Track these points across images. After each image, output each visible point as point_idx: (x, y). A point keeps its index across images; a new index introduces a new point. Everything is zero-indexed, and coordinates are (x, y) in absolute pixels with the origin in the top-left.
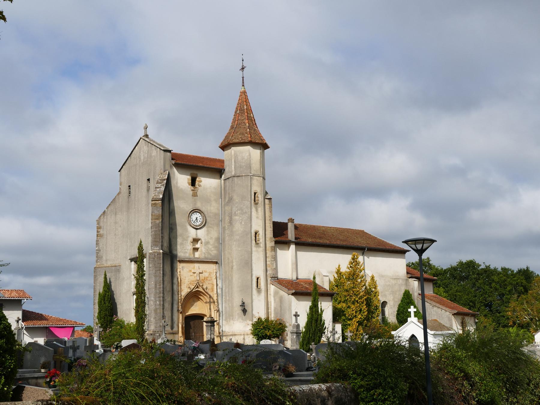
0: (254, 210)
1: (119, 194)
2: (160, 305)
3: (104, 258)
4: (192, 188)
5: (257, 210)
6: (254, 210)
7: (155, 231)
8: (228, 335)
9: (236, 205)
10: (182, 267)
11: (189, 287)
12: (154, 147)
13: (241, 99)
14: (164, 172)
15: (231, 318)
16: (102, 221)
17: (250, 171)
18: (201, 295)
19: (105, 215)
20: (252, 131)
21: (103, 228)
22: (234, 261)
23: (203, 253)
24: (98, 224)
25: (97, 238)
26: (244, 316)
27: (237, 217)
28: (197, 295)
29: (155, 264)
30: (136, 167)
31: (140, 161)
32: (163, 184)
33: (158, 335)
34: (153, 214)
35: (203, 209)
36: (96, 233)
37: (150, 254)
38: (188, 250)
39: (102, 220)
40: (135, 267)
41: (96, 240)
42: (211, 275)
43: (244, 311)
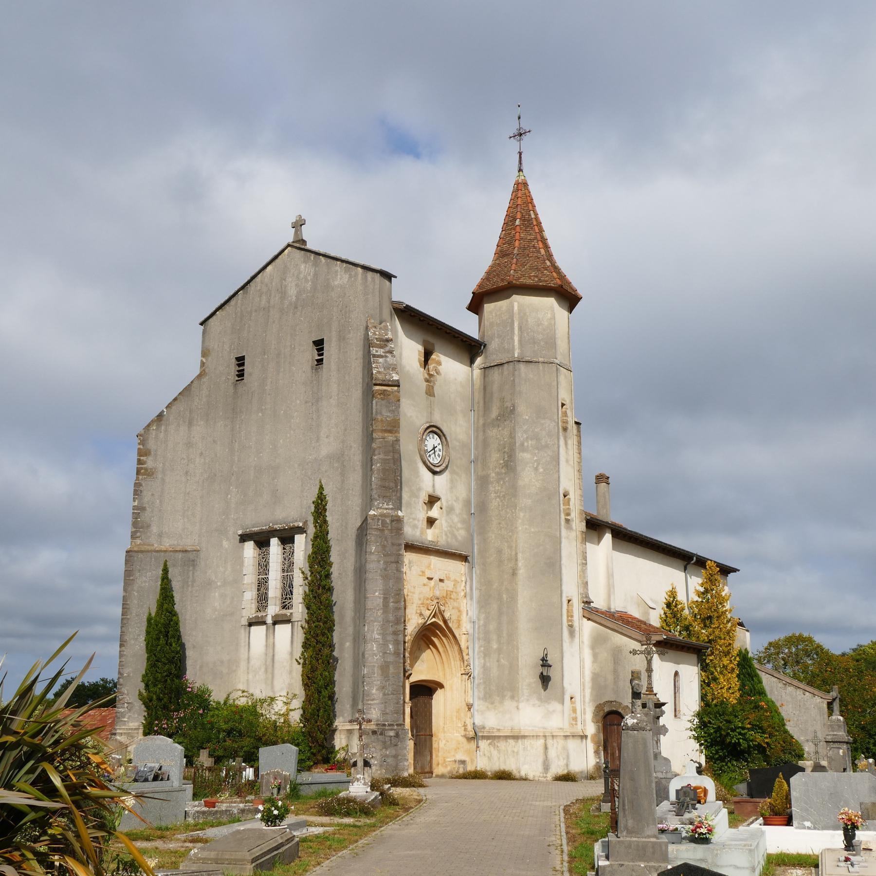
1: (200, 376)
2: (396, 653)
3: (154, 529)
8: (500, 736)
9: (525, 427)
11: (421, 614)
15: (509, 694)
18: (436, 636)
21: (156, 455)
22: (520, 556)
23: (444, 533)
24: (143, 442)
25: (137, 479)
26: (545, 691)
27: (526, 456)
28: (429, 634)
29: (384, 547)
30: (269, 311)
33: (392, 733)
36: (134, 465)
40: (255, 556)
41: (135, 483)
42: (456, 588)
43: (545, 680)
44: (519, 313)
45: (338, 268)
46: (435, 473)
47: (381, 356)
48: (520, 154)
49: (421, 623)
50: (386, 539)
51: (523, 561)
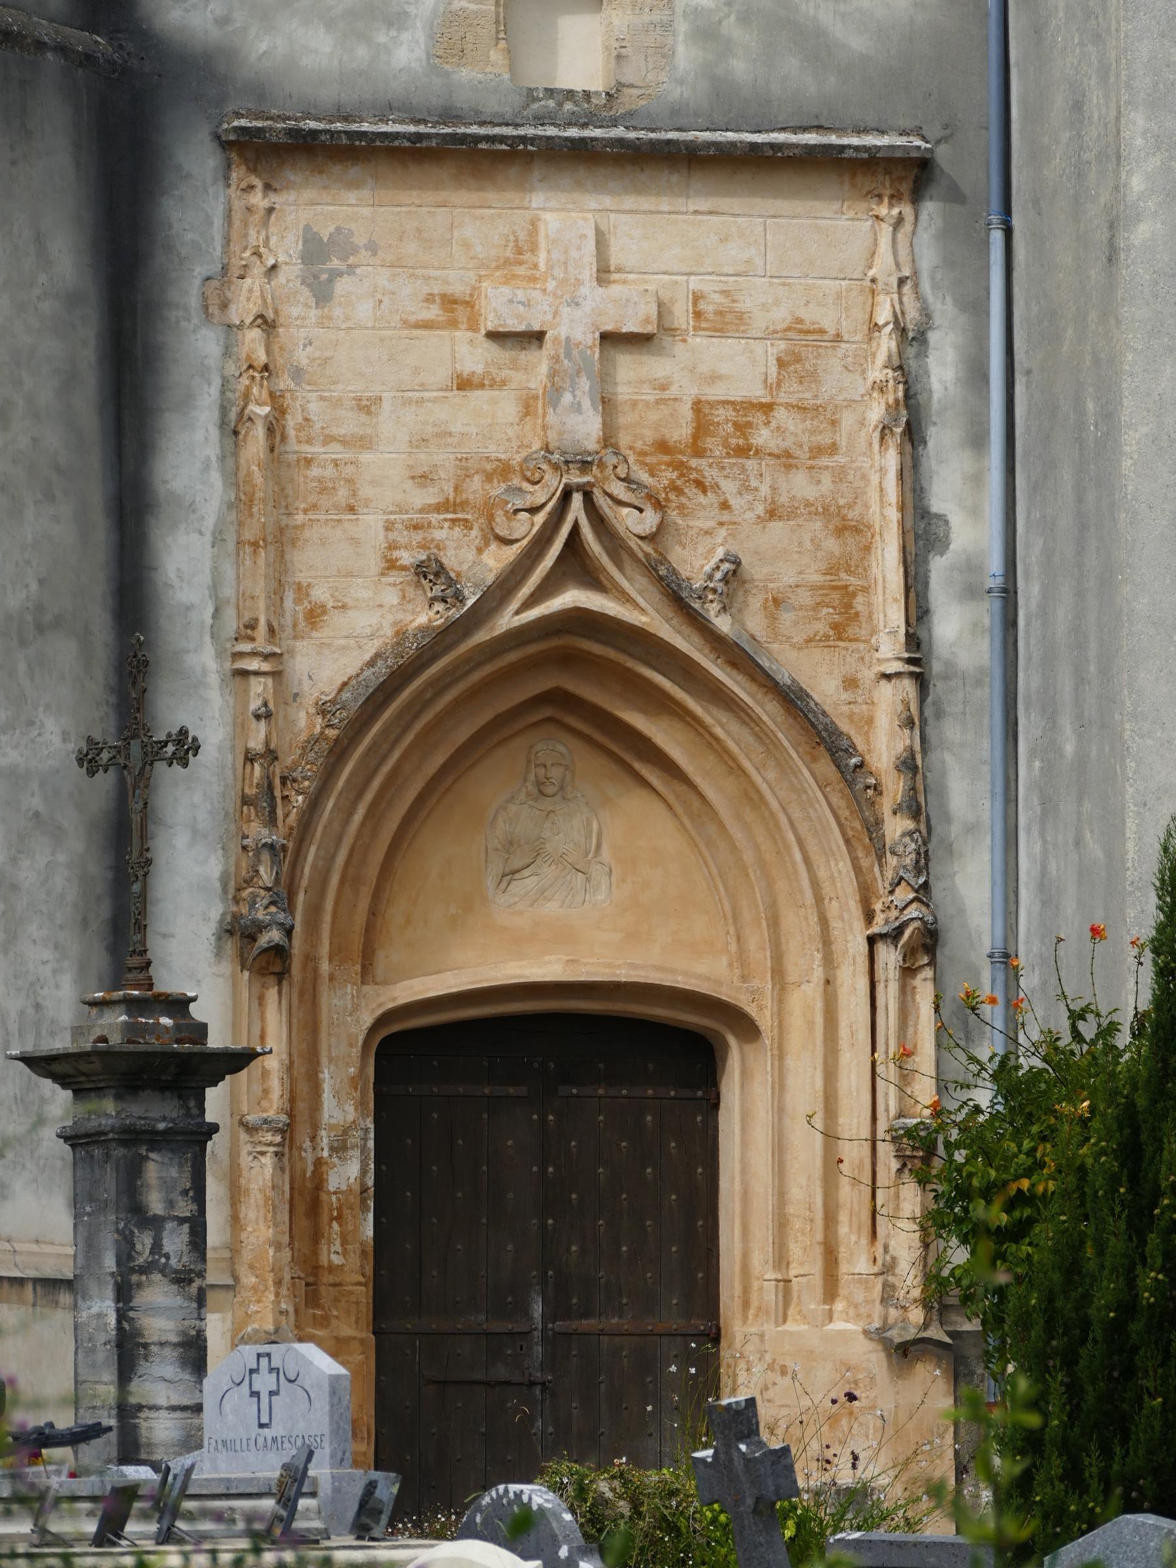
23: (682, 27)
49: (423, 629)
51: (1155, 162)
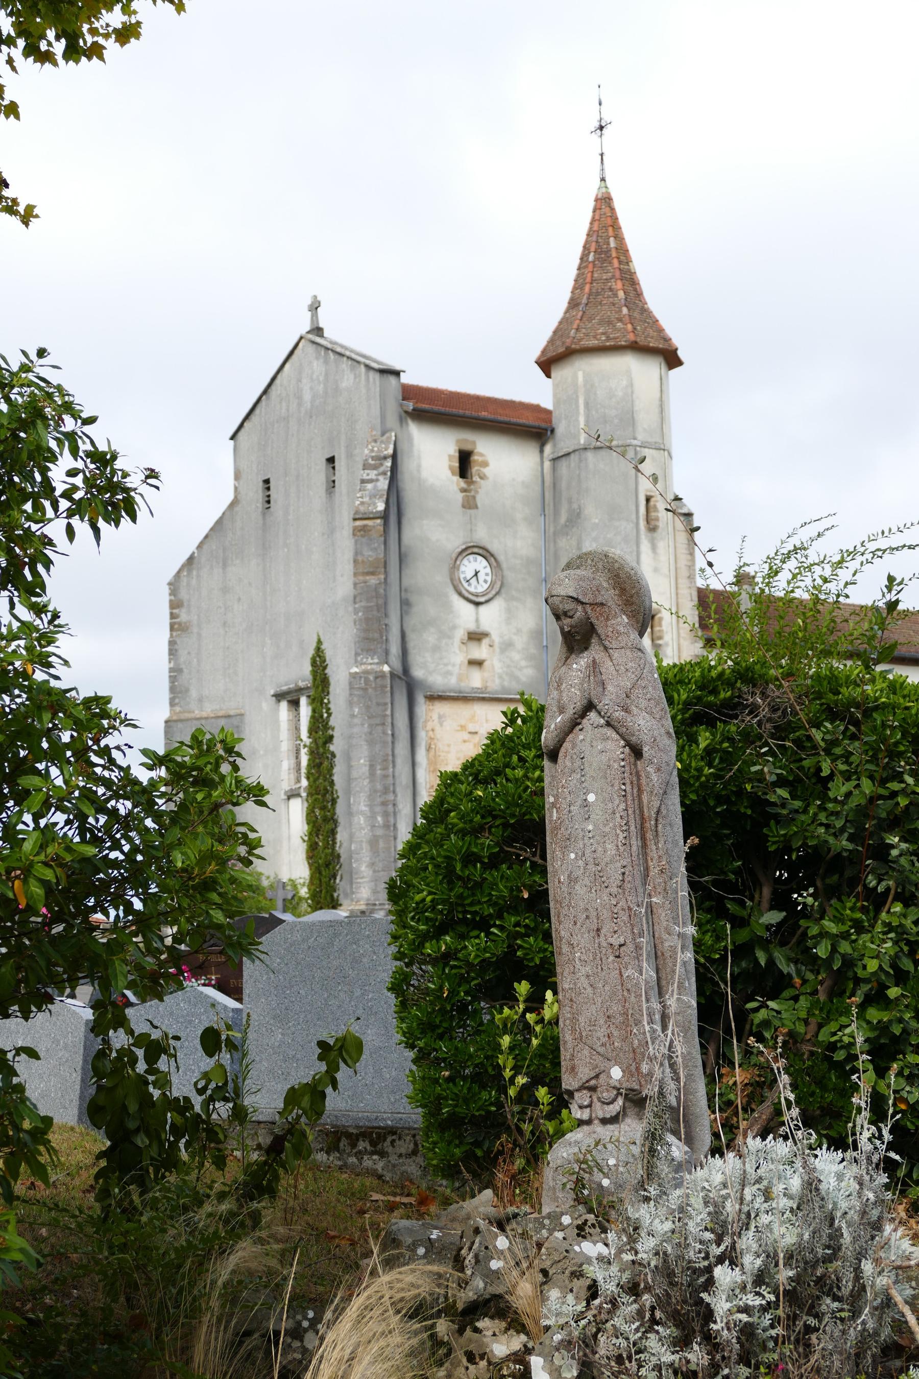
0: (645, 546)
1: (232, 505)
3: (194, 693)
4: (462, 483)
5: (654, 548)
6: (645, 546)
7: (367, 609)
9: (594, 534)
10: (440, 717)
12: (345, 365)
13: (597, 217)
14: (383, 434)
16: (185, 584)
17: (634, 431)
19: (194, 566)
20: (636, 314)
21: (189, 606)
25: (171, 636)
30: (288, 422)
31: (300, 405)
32: (382, 469)
34: (360, 558)
35: (494, 547)
37: (354, 678)
38: (454, 665)
39: (184, 581)
44: (585, 385)
45: (344, 366)
46: (477, 604)
47: (370, 481)
48: (602, 155)
50: (370, 699)
